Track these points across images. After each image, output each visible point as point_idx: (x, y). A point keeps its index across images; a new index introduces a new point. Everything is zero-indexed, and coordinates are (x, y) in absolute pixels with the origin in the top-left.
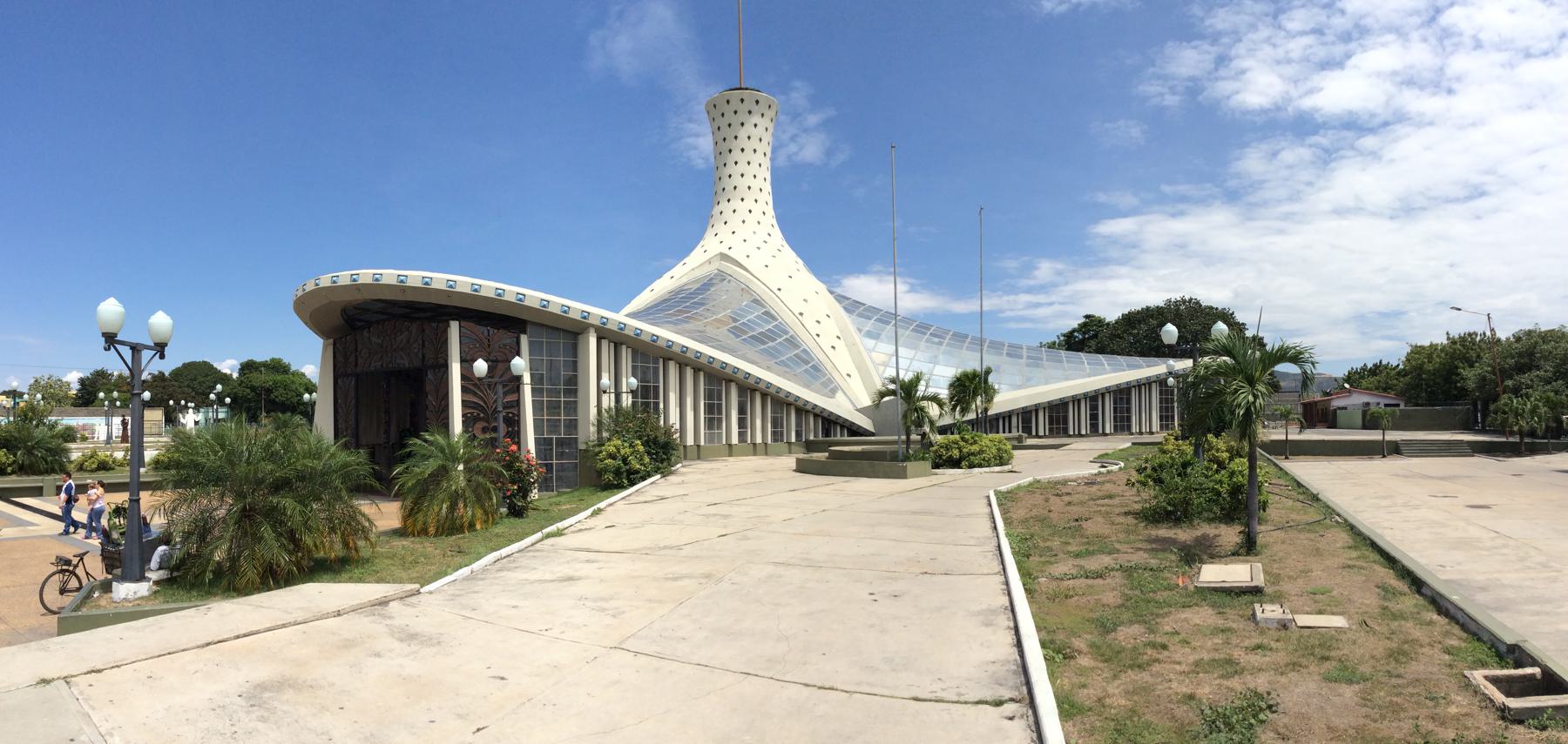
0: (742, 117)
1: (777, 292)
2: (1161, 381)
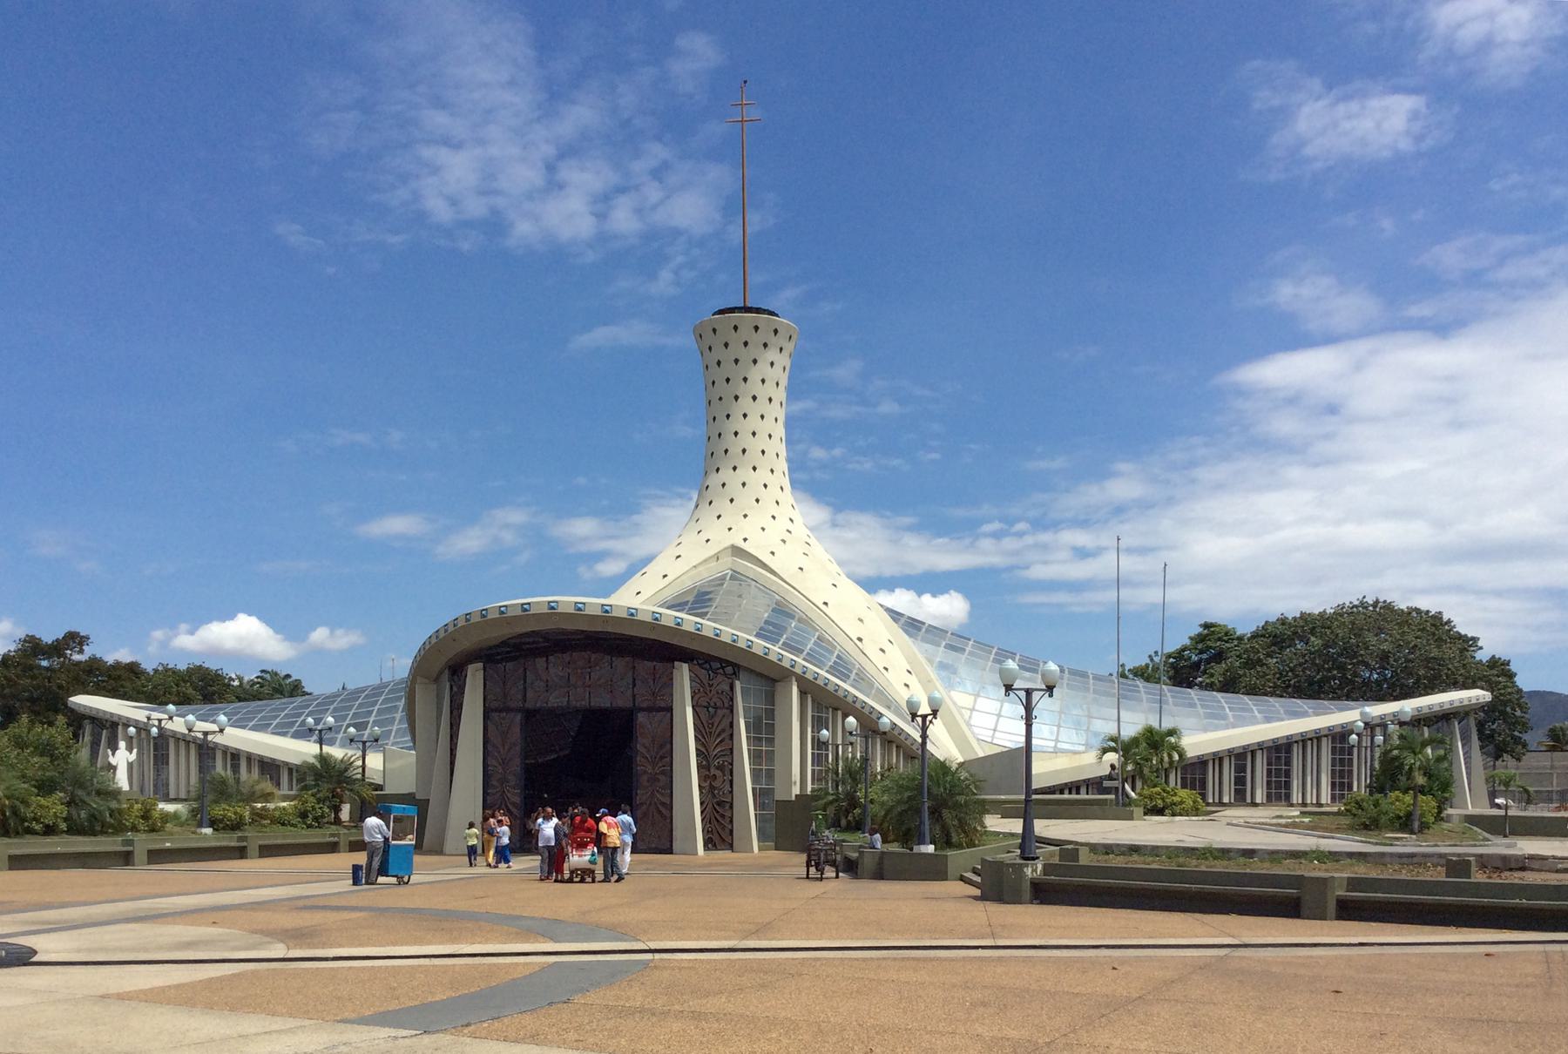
0: (753, 351)
1: (823, 607)
2: (1339, 736)
